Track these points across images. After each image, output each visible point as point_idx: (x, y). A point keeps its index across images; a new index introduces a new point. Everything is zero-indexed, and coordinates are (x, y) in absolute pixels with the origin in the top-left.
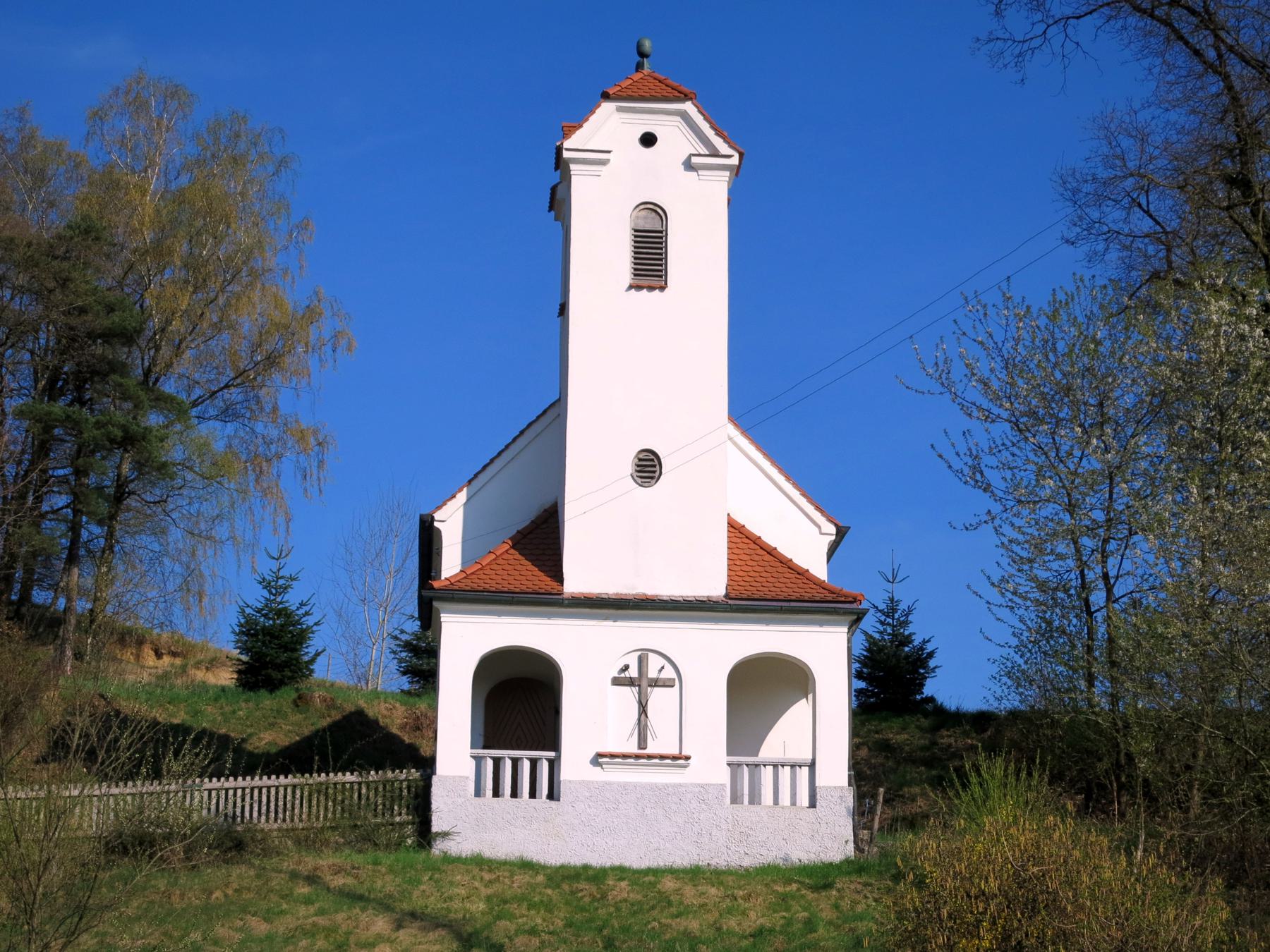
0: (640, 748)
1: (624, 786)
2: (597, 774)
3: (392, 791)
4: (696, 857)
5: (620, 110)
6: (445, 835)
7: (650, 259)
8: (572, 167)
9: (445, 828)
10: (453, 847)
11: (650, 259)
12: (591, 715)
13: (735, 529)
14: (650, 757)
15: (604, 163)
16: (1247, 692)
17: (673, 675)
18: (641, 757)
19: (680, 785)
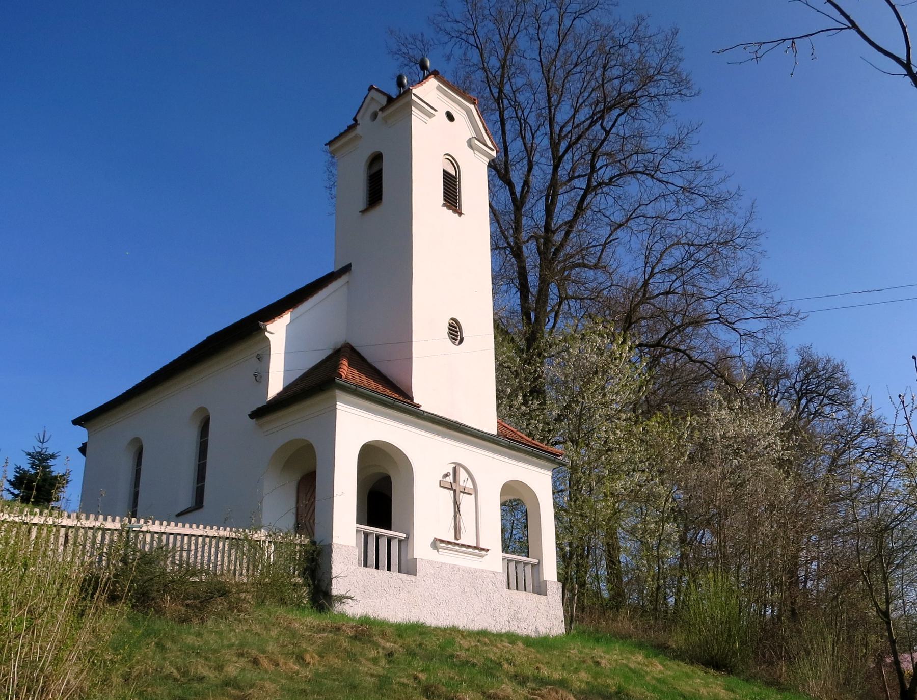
0: (456, 538)
1: (453, 567)
2: (433, 555)
3: (128, 540)
4: (486, 624)
5: (438, 88)
6: (341, 598)
7: (452, 194)
8: (490, 426)
9: (343, 592)
10: (353, 609)
11: (452, 194)
12: (428, 510)
13: (460, 214)
14: (462, 545)
15: (430, 116)
16: (890, 516)
17: (469, 485)
18: (455, 544)
19: (483, 570)
